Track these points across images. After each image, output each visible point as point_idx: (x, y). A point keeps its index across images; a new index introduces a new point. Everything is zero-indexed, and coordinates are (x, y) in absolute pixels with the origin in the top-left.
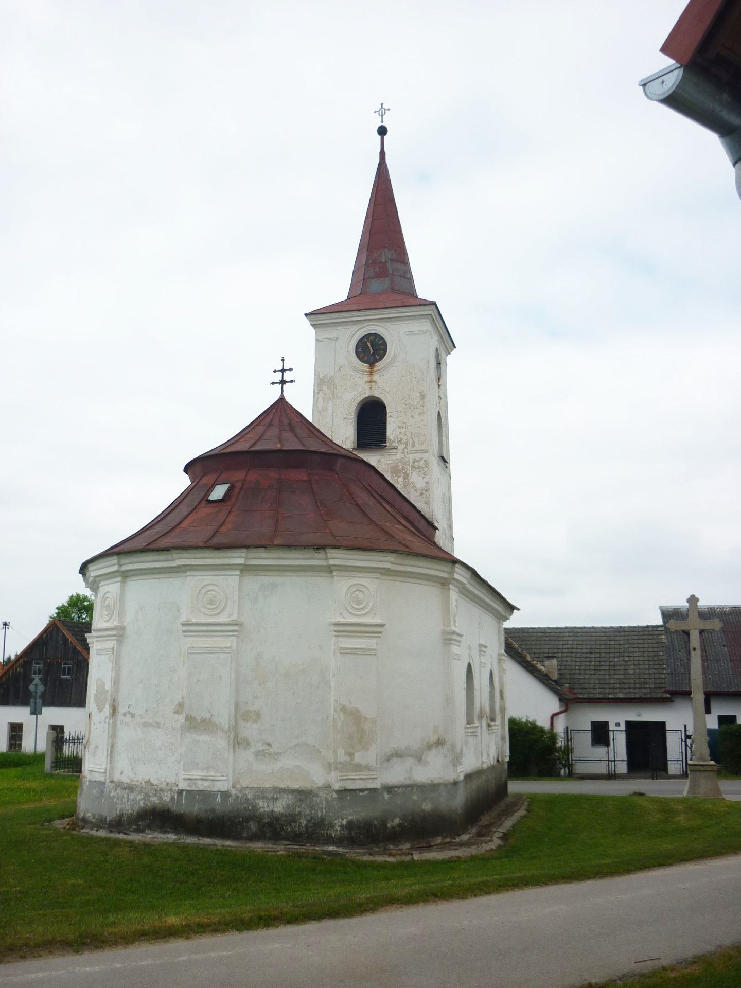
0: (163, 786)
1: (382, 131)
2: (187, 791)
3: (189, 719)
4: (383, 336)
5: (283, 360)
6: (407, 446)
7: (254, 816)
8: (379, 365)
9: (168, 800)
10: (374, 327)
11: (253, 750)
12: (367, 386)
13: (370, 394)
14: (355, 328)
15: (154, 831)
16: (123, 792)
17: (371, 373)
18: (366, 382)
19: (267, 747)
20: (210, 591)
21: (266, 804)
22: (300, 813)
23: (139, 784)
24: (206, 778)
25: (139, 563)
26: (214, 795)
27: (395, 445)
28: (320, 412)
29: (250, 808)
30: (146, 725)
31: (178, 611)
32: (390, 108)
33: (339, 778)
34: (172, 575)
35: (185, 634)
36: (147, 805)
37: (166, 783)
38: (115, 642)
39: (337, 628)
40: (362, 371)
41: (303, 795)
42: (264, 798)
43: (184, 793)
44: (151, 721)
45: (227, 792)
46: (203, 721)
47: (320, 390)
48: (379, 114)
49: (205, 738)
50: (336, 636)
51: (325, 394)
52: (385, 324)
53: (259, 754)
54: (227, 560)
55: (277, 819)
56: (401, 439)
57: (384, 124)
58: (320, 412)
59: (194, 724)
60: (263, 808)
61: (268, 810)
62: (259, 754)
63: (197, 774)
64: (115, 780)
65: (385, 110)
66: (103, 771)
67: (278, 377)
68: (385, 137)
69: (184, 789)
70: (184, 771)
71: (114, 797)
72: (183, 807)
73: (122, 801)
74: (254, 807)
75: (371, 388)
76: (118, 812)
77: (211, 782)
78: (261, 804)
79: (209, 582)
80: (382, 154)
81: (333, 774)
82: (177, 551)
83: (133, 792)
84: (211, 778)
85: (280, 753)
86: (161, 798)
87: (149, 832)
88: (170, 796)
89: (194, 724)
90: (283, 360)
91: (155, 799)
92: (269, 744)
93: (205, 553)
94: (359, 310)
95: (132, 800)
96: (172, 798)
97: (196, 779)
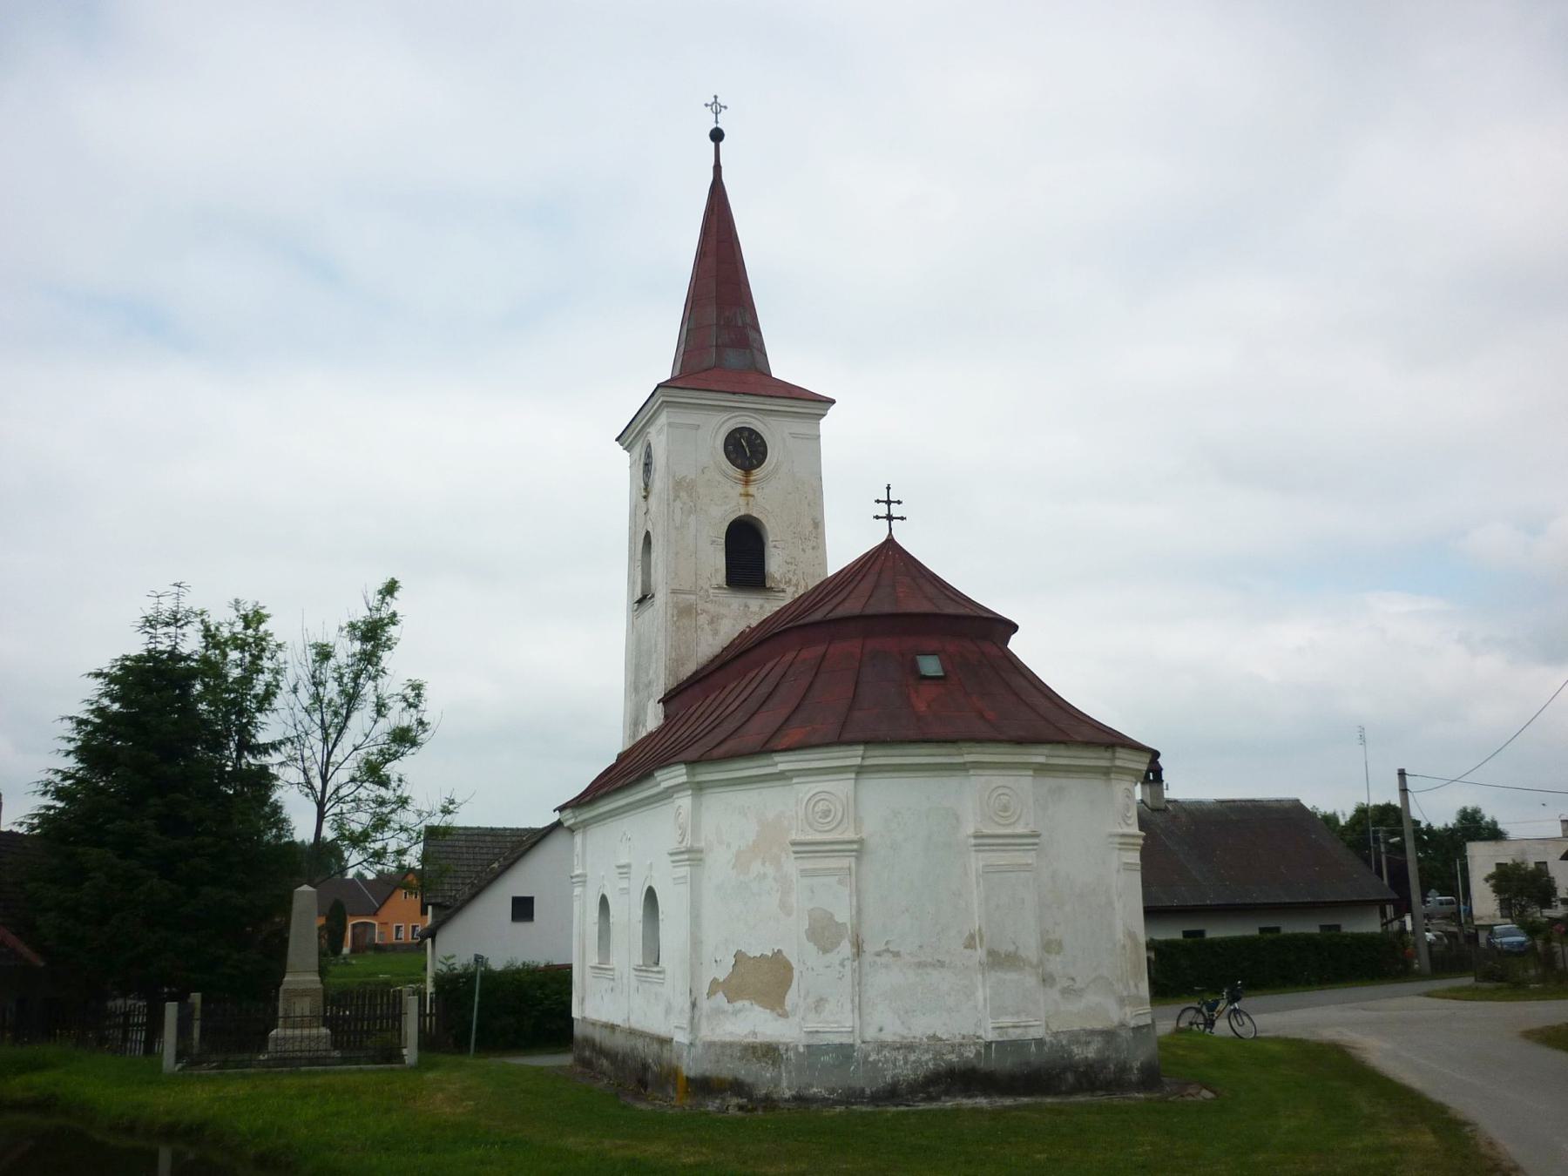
0: (958, 1040)
1: (717, 136)
2: (997, 1042)
3: (991, 953)
4: (762, 434)
5: (888, 488)
6: (797, 589)
7: (1071, 1066)
8: (757, 473)
9: (972, 1056)
10: (749, 420)
11: (1058, 987)
12: (742, 501)
13: (747, 512)
14: (725, 416)
15: (955, 1097)
16: (895, 1053)
17: (747, 483)
18: (741, 495)
19: (1071, 983)
20: (1003, 794)
21: (1080, 1049)
22: (1108, 1057)
23: (917, 1040)
24: (1018, 1024)
25: (884, 756)
26: (1028, 1044)
27: (782, 586)
28: (677, 528)
29: (1066, 1056)
30: (921, 965)
31: (957, 819)
32: (728, 106)
33: (1134, 1014)
34: (946, 773)
35: (977, 848)
36: (940, 1065)
37: (961, 1036)
38: (688, 868)
39: (1123, 840)
40: (736, 478)
41: (1109, 1035)
42: (1078, 1042)
43: (994, 1045)
44: (930, 960)
45: (1041, 1039)
46: (1008, 956)
47: (677, 497)
48: (712, 109)
49: (1012, 976)
50: (976, 851)
51: (684, 504)
52: (766, 418)
53: (1065, 992)
54: (1025, 757)
55: (1091, 1066)
56: (790, 580)
57: (719, 126)
58: (677, 528)
59: (1000, 960)
60: (1078, 1054)
61: (1082, 1056)
62: (1065, 992)
63: (1006, 1020)
64: (868, 1039)
65: (721, 106)
66: (850, 1029)
67: (882, 510)
68: (721, 144)
69: (994, 1040)
70: (992, 1018)
71: (875, 1063)
72: (994, 1063)
73: (895, 1065)
74: (1070, 1053)
75: (748, 504)
76: (888, 1079)
77: (1023, 1029)
78: (1076, 1050)
79: (1000, 784)
80: (717, 168)
81: (1128, 1010)
82: (968, 745)
83: (914, 1052)
84: (1023, 1024)
85: (1082, 989)
86: (962, 1055)
87: (948, 1098)
88: (974, 1051)
89: (1000, 960)
90: (888, 488)
91: (953, 1058)
92: (1073, 979)
93: (923, 748)
94: (734, 393)
95: (914, 1062)
96: (978, 1054)
97: (1008, 1027)
